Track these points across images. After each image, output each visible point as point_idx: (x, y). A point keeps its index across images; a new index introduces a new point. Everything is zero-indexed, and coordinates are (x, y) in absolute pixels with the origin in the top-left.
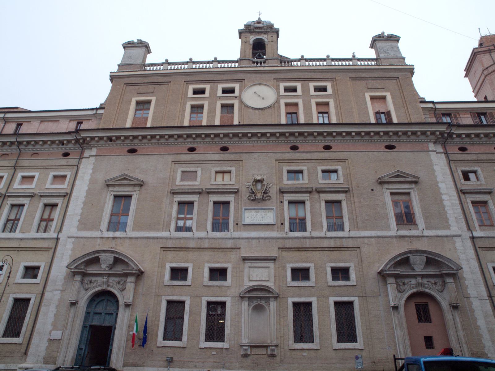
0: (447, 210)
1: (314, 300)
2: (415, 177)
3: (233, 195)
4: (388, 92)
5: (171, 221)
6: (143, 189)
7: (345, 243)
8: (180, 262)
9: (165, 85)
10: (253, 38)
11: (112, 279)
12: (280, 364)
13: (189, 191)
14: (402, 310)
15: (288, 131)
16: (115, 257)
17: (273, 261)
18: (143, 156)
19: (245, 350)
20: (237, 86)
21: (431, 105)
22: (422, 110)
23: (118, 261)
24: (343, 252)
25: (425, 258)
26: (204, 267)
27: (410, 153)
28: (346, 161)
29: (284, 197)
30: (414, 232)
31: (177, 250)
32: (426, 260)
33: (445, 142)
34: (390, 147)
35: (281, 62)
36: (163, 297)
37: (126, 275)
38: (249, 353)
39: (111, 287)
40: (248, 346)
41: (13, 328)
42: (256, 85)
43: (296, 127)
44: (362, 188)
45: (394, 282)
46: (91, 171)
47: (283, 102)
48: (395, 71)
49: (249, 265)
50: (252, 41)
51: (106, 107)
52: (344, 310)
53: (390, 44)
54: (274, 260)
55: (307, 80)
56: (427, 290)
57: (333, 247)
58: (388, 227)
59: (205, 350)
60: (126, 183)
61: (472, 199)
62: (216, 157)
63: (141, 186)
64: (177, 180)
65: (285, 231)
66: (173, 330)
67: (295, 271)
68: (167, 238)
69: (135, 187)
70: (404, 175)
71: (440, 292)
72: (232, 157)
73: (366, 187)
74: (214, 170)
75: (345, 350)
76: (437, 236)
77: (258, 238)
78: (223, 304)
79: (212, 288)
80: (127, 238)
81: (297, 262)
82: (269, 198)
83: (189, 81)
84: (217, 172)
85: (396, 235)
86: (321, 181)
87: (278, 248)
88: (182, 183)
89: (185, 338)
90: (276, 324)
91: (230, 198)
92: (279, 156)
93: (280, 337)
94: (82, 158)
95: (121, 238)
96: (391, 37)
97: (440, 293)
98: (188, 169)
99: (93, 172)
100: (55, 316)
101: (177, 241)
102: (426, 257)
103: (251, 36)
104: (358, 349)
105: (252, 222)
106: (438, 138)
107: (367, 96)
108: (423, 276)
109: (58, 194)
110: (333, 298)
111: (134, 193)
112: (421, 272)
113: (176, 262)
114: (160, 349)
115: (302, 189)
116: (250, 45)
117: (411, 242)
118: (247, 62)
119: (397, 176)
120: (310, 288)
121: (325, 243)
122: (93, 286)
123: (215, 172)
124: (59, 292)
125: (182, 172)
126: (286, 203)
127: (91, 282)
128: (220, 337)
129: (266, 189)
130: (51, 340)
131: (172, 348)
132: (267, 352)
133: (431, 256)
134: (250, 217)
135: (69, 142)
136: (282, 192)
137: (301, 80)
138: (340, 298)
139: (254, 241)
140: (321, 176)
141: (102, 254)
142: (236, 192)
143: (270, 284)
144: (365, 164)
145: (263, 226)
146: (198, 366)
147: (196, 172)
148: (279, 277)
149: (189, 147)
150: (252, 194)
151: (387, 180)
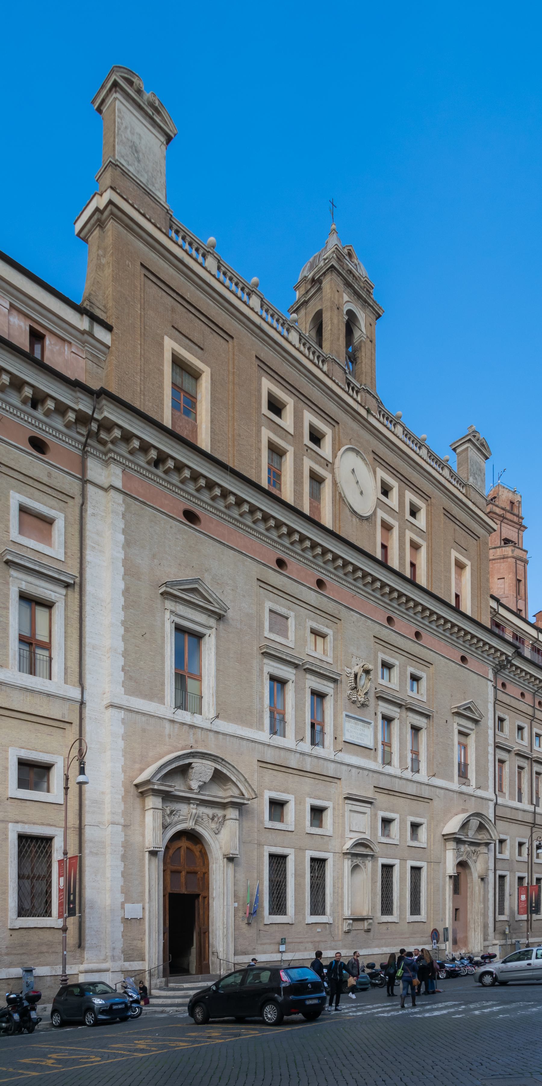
16: (216, 769)
19: (349, 924)
25: (479, 822)
29: (379, 707)
36: (266, 847)
41: (33, 899)
49: (350, 807)
61: (24, 586)
72: (331, 607)
80: (210, 731)
100: (123, 876)
109: (56, 576)
124: (120, 828)
130: (126, 921)
147: (287, 618)
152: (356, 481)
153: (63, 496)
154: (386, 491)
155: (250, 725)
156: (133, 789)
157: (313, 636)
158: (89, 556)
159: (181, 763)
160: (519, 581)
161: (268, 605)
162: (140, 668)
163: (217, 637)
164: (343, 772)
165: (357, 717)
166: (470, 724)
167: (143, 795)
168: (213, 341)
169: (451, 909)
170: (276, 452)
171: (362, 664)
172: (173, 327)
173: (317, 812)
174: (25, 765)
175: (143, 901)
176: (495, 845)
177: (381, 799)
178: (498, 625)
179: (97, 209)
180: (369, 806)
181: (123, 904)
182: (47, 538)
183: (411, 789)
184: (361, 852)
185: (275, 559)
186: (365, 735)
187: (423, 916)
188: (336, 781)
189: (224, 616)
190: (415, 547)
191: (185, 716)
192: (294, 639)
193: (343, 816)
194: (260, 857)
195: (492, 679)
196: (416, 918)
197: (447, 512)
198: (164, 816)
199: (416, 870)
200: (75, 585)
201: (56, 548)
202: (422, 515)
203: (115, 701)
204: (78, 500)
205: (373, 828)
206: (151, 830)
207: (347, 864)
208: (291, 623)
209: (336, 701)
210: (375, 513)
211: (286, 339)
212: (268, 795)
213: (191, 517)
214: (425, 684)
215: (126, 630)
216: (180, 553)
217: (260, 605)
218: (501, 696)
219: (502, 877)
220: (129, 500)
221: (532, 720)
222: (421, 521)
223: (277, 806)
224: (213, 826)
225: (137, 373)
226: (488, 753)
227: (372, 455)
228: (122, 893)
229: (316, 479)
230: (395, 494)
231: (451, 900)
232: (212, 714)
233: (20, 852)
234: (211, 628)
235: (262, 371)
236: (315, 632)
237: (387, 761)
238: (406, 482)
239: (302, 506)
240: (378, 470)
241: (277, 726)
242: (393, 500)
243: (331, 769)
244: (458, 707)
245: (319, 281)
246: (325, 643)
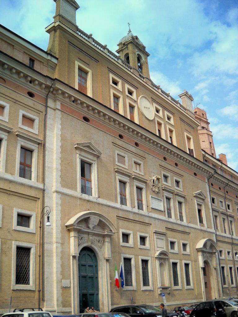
16: (100, 220)
41: (22, 277)
45: (77, 236)
51: (59, 59)
61: (23, 144)
72: (141, 153)
74: (134, 159)
79: (143, 251)
80: (96, 203)
86: (20, 126)
100: (61, 267)
135: (40, 84)
147: (124, 157)
152: (147, 109)
153: (38, 112)
154: (158, 111)
155: (113, 201)
156: (65, 228)
157: (135, 164)
158: (48, 133)
159: (86, 217)
160: (211, 143)
161: (117, 152)
163: (98, 165)
164: (152, 221)
166: (201, 201)
167: (69, 231)
168: (92, 63)
169: (204, 283)
170: (116, 98)
171: (156, 176)
173: (143, 239)
174: (20, 215)
175: (70, 278)
176: (218, 253)
177: (169, 233)
178: (206, 161)
179: (54, 26)
180: (165, 236)
181: (61, 280)
182: (32, 126)
183: (180, 229)
184: (163, 257)
185: (118, 135)
186: (161, 206)
187: (192, 286)
188: (149, 225)
189: (100, 156)
190: (171, 131)
191: (85, 196)
192: (128, 165)
195: (207, 182)
196: (189, 287)
197: (181, 119)
199: (187, 265)
200: (42, 145)
201: (35, 130)
202: (172, 119)
204: (44, 113)
205: (167, 246)
206: (73, 247)
207: (157, 263)
208: (126, 159)
209: (146, 191)
210: (154, 118)
211: (118, 63)
212: (121, 231)
213: (86, 119)
214: (182, 184)
215: (62, 161)
216: (82, 133)
217: (114, 152)
218: (212, 189)
219: (223, 268)
220: (63, 113)
221: (225, 199)
222: (172, 121)
223: (126, 236)
224: (99, 244)
225: (66, 72)
226: (210, 213)
227: (151, 99)
228: (61, 274)
229: (132, 107)
230: (161, 112)
231: (203, 279)
233: (17, 254)
234: (95, 161)
235: (109, 71)
236: (136, 163)
237: (170, 216)
238: (165, 108)
239: (127, 116)
240: (154, 104)
241: (123, 201)
242: (161, 114)
243: (147, 220)
244: (196, 194)
245: (127, 45)
246: (140, 168)
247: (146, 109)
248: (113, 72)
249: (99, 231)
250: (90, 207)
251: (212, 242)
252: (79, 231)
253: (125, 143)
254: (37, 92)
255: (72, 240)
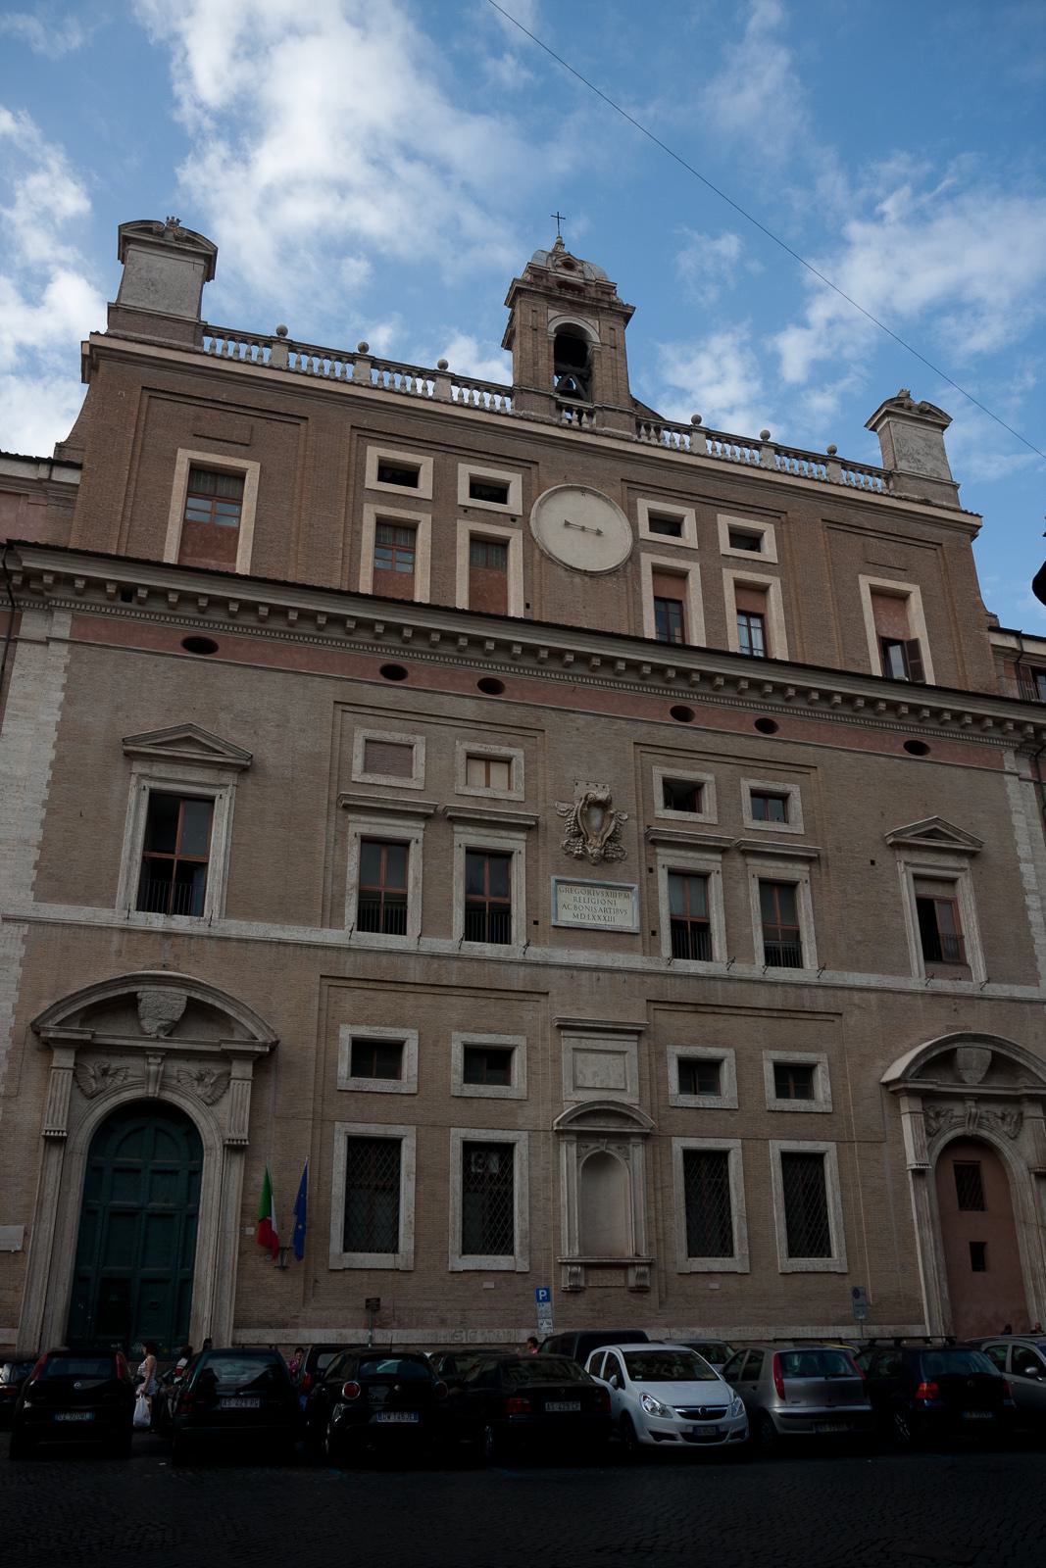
0: (1035, 936)
1: (734, 1145)
2: (973, 841)
3: (522, 836)
4: (915, 583)
5: (343, 896)
6: (249, 781)
7: (807, 1000)
8: (380, 1025)
9: (288, 426)
10: (556, 318)
11: (176, 1067)
12: (659, 1311)
13: (398, 808)
14: (931, 1179)
15: (675, 664)
17: (635, 1037)
18: (238, 670)
19: (574, 1275)
20: (515, 482)
21: (1012, 643)
22: (994, 652)
23: (199, 1011)
24: (801, 1023)
25: (989, 1054)
26: (449, 1041)
27: (960, 772)
28: (811, 771)
29: (659, 857)
30: (964, 987)
31: (371, 985)
32: (993, 1059)
33: (1038, 754)
34: (916, 748)
35: (638, 426)
37: (226, 1057)
38: (582, 1284)
39: (174, 1090)
40: (580, 1264)
42: (572, 489)
43: (697, 657)
44: (850, 854)
46: (60, 696)
47: (647, 560)
48: (936, 523)
49: (574, 1043)
50: (552, 328)
51: (86, 465)
52: (802, 1171)
53: (923, 434)
54: (639, 1033)
55: (711, 501)
56: (985, 1133)
57: (780, 1008)
58: (904, 969)
59: (465, 1277)
60: (195, 756)
61: (365, 830)
62: (469, 708)
63: (243, 770)
64: (354, 767)
65: (660, 956)
66: (371, 1227)
67: (687, 1066)
68: (338, 949)
69: (221, 773)
70: (949, 833)
71: (1011, 1139)
72: (515, 715)
73: (858, 853)
74: (463, 747)
75: (806, 1276)
76: (1013, 1000)
77: (596, 969)
78: (506, 1150)
80: (210, 937)
81: (694, 1042)
82: (620, 854)
83: (365, 429)
84: (471, 757)
85: (924, 988)
86: (751, 826)
87: (647, 1001)
88: (369, 778)
89: (406, 1241)
90: (633, 1208)
91: (515, 842)
92: (642, 732)
93: (657, 1240)
94: (15, 641)
95: (191, 936)
96: (928, 412)
97: (1011, 1141)
98: (387, 736)
99: (69, 701)
101: (370, 959)
102: (994, 1053)
103: (552, 313)
104: (835, 1272)
105: (576, 920)
106: (1028, 741)
107: (865, 583)
108: (981, 1099)
110: (780, 1142)
111: (222, 791)
112: (975, 1087)
113: (369, 1022)
114: (340, 1276)
115: (705, 840)
116: (549, 341)
117: (955, 1010)
118: (545, 402)
119: (930, 835)
120: (726, 1114)
121: (761, 998)
122: (114, 1085)
123: (464, 756)
125: (368, 741)
126: (662, 875)
127: (105, 1072)
128: (501, 1242)
129: (614, 831)
131: (372, 1273)
132: (626, 1280)
133: (1004, 1052)
134: (577, 906)
136: (655, 843)
137: (695, 498)
138: (795, 1142)
139: (585, 975)
140: (750, 803)
141: (147, 988)
142: (530, 829)
143: (629, 1098)
144: (850, 789)
145: (608, 935)
146: (449, 1321)
147: (411, 747)
148: (651, 1080)
149: (385, 663)
150: (574, 837)
151: (909, 841)
159: (944, 1049)
162: (71, 860)
165: (595, 882)
172: (195, 435)
193: (557, 1061)
194: (324, 1146)
198: (926, 1121)
203: (10, 913)
207: (568, 1156)
232: (983, 979)
234: (963, 870)
247: (571, 534)
248: (389, 438)
249: (999, 1086)
250: (177, 957)
251: (994, 1043)
252: (927, 1097)
253: (413, 693)
254: (488, 669)
255: (906, 1123)
